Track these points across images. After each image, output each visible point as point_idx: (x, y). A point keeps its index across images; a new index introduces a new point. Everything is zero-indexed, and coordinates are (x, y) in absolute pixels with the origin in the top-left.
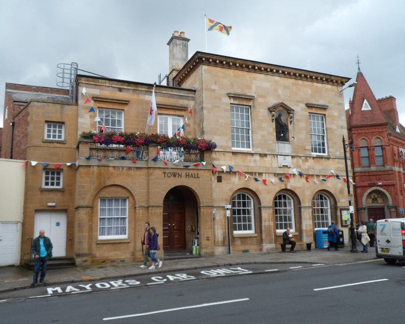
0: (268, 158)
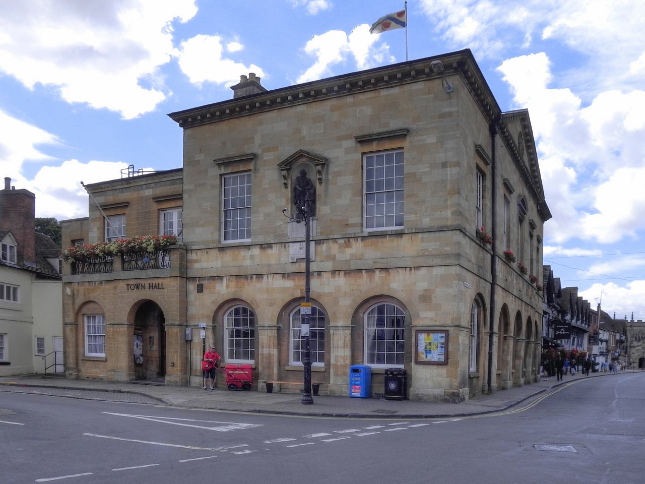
0: (275, 250)
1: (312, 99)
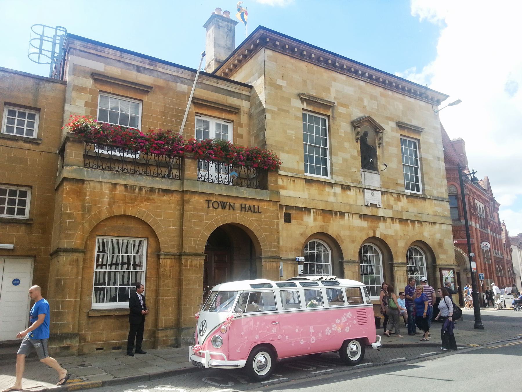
0: (352, 193)
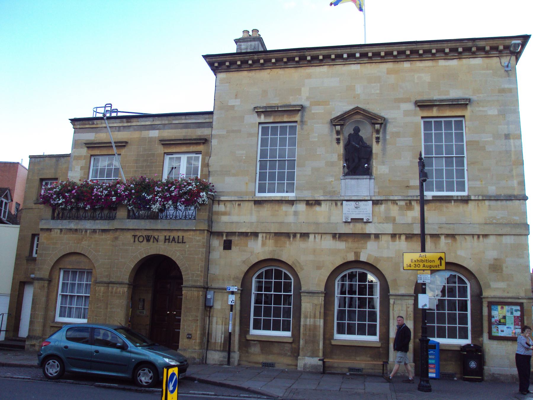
0: (324, 208)
1: (368, 60)
